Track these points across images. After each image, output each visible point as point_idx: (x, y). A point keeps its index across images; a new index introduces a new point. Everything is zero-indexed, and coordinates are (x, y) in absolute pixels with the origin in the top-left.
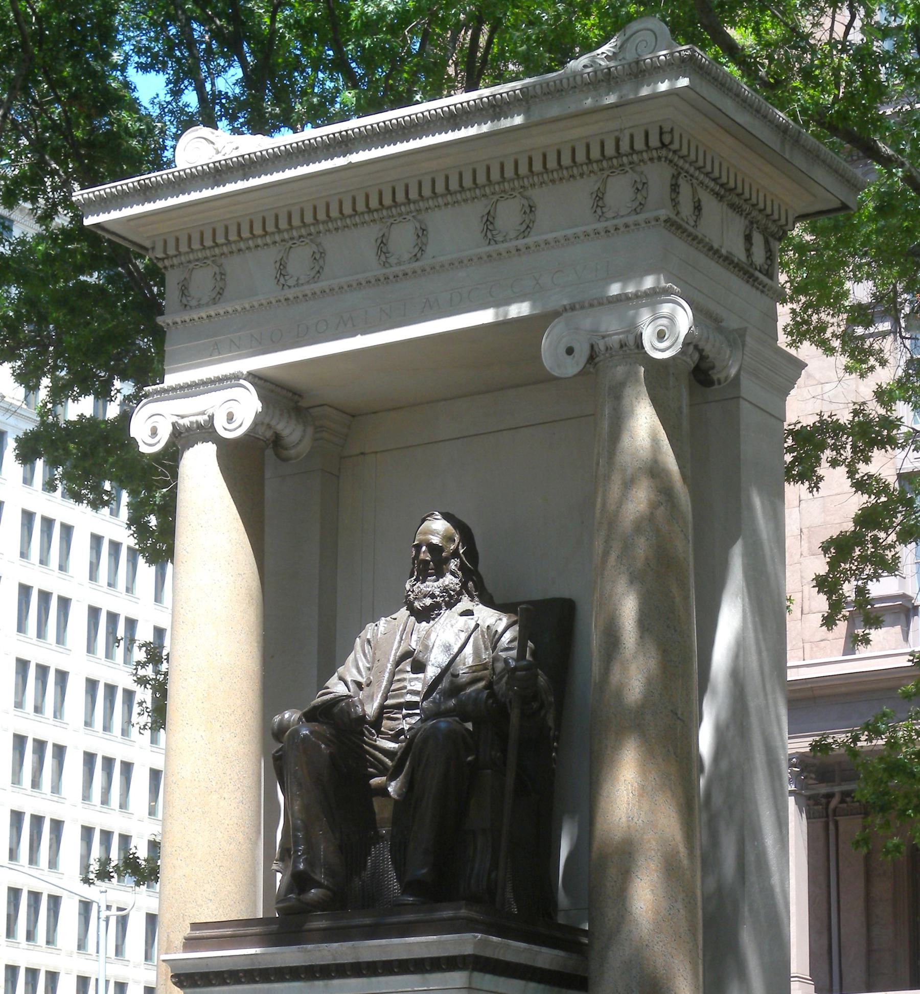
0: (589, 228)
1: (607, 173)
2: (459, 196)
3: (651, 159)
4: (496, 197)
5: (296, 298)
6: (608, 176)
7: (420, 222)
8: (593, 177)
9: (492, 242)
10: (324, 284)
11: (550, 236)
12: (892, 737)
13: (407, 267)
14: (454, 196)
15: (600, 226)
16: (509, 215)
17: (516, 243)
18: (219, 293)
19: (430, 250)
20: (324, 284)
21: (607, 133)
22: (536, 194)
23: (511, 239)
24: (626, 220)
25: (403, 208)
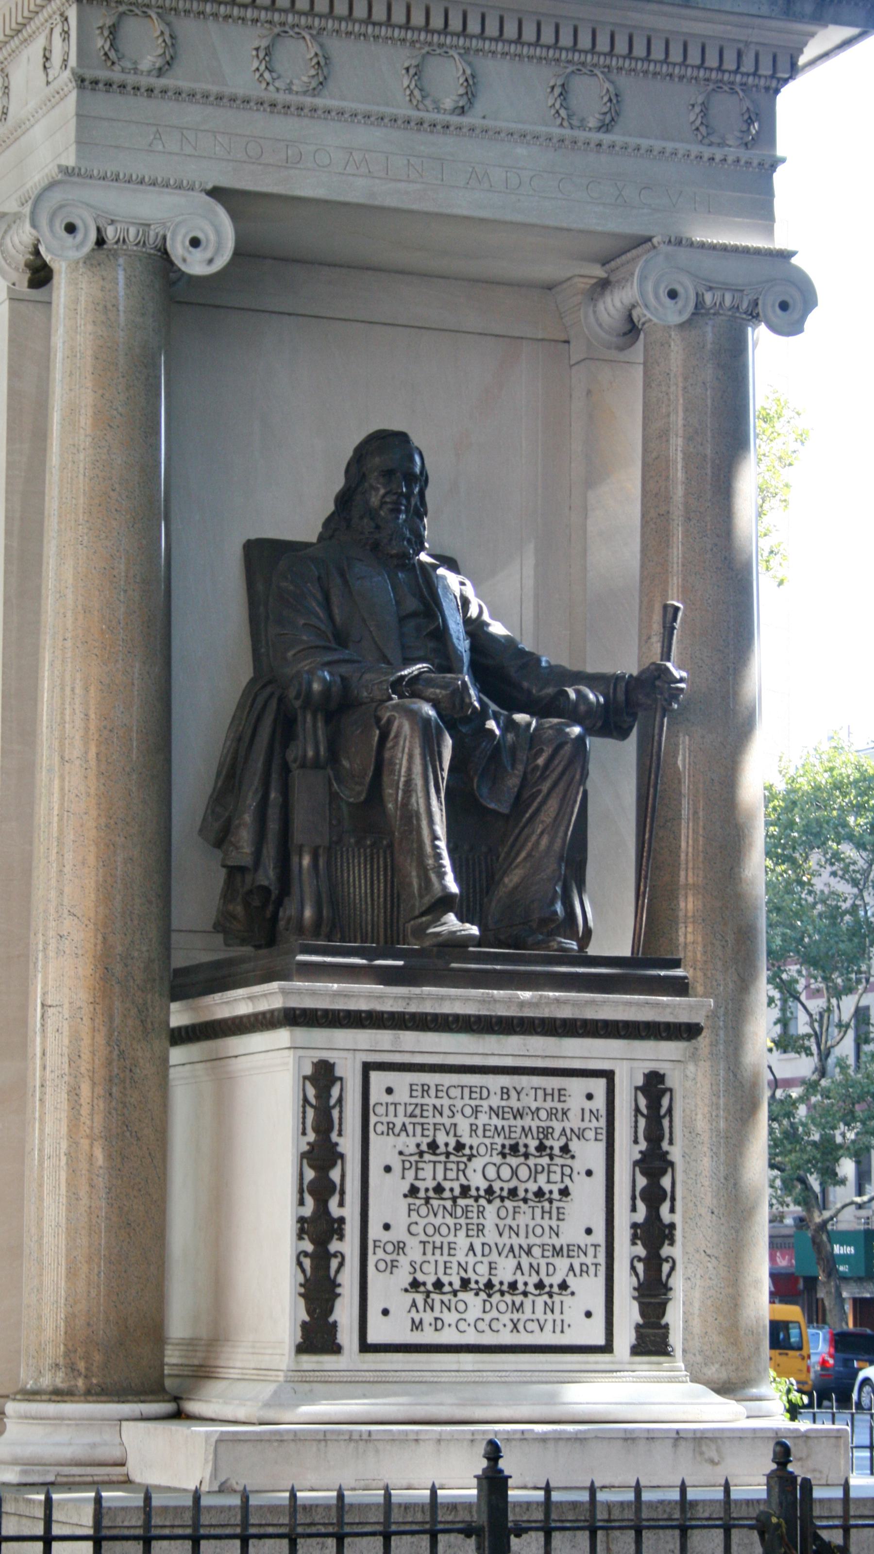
0: (542, 129)
1: (711, 86)
2: (303, 20)
3: (646, 72)
4: (571, 68)
5: (625, 147)
6: (573, 72)
7: (322, 46)
8: (259, 30)
9: (565, 124)
10: (319, 102)
11: (633, 141)
12: (706, 1364)
13: (145, 81)
14: (377, 28)
15: (556, 131)
16: (589, 95)
17: (448, 118)
18: (168, 63)
19: (480, 106)
20: (319, 102)
21: (729, 40)
22: (338, 47)
23: (590, 129)
24: (448, 118)
25: (397, 31)
